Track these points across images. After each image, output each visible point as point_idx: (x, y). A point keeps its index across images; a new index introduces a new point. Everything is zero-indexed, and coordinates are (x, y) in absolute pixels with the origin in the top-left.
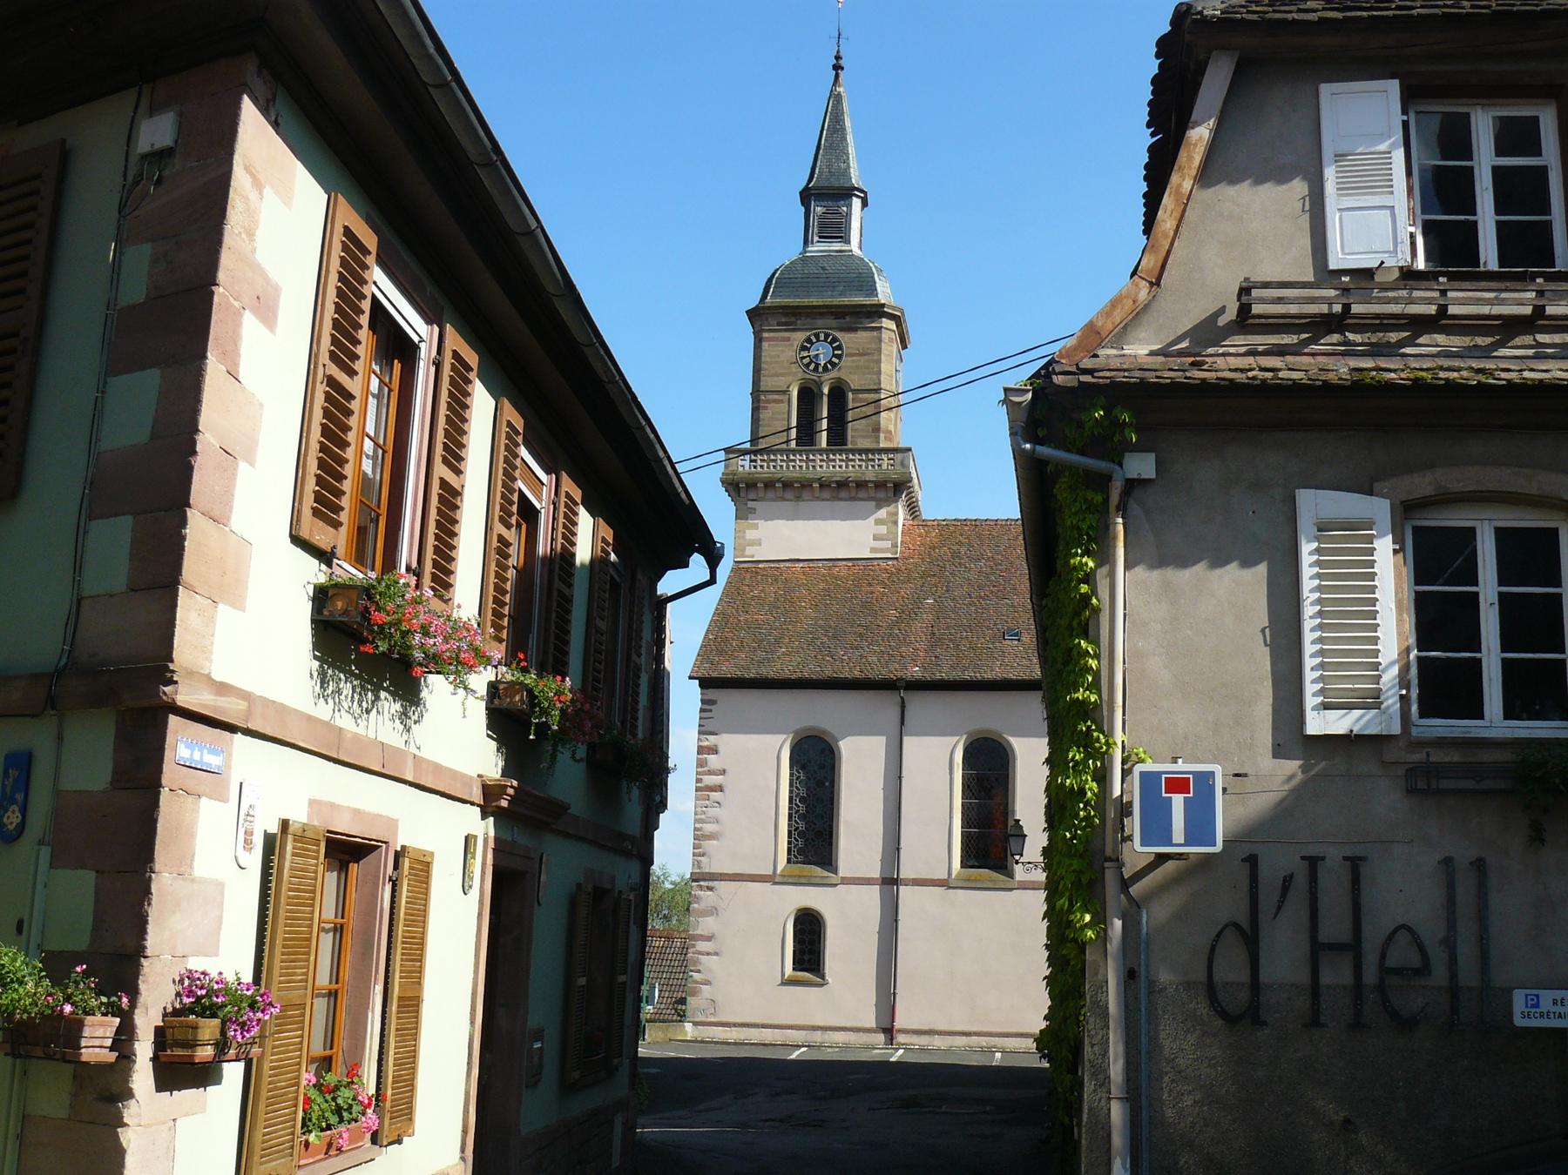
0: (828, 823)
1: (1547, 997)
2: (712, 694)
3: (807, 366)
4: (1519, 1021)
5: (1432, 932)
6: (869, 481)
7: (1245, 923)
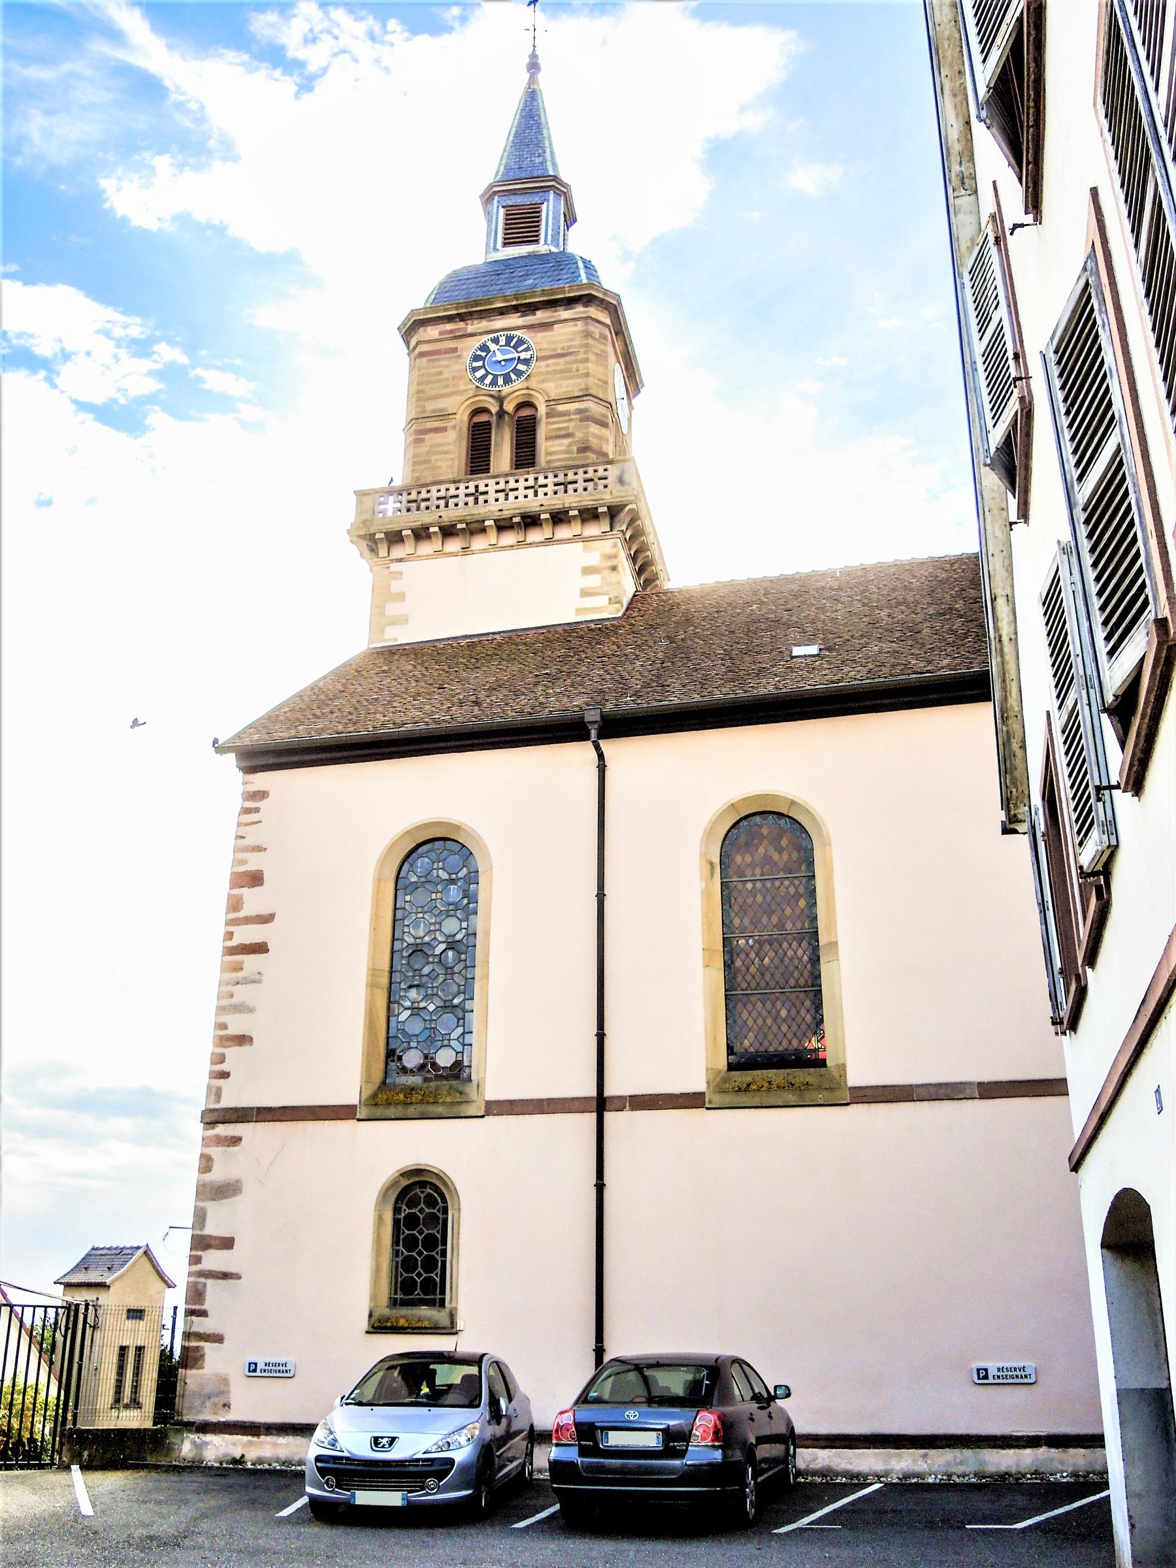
2: (263, 780)
3: (482, 379)
6: (570, 509)
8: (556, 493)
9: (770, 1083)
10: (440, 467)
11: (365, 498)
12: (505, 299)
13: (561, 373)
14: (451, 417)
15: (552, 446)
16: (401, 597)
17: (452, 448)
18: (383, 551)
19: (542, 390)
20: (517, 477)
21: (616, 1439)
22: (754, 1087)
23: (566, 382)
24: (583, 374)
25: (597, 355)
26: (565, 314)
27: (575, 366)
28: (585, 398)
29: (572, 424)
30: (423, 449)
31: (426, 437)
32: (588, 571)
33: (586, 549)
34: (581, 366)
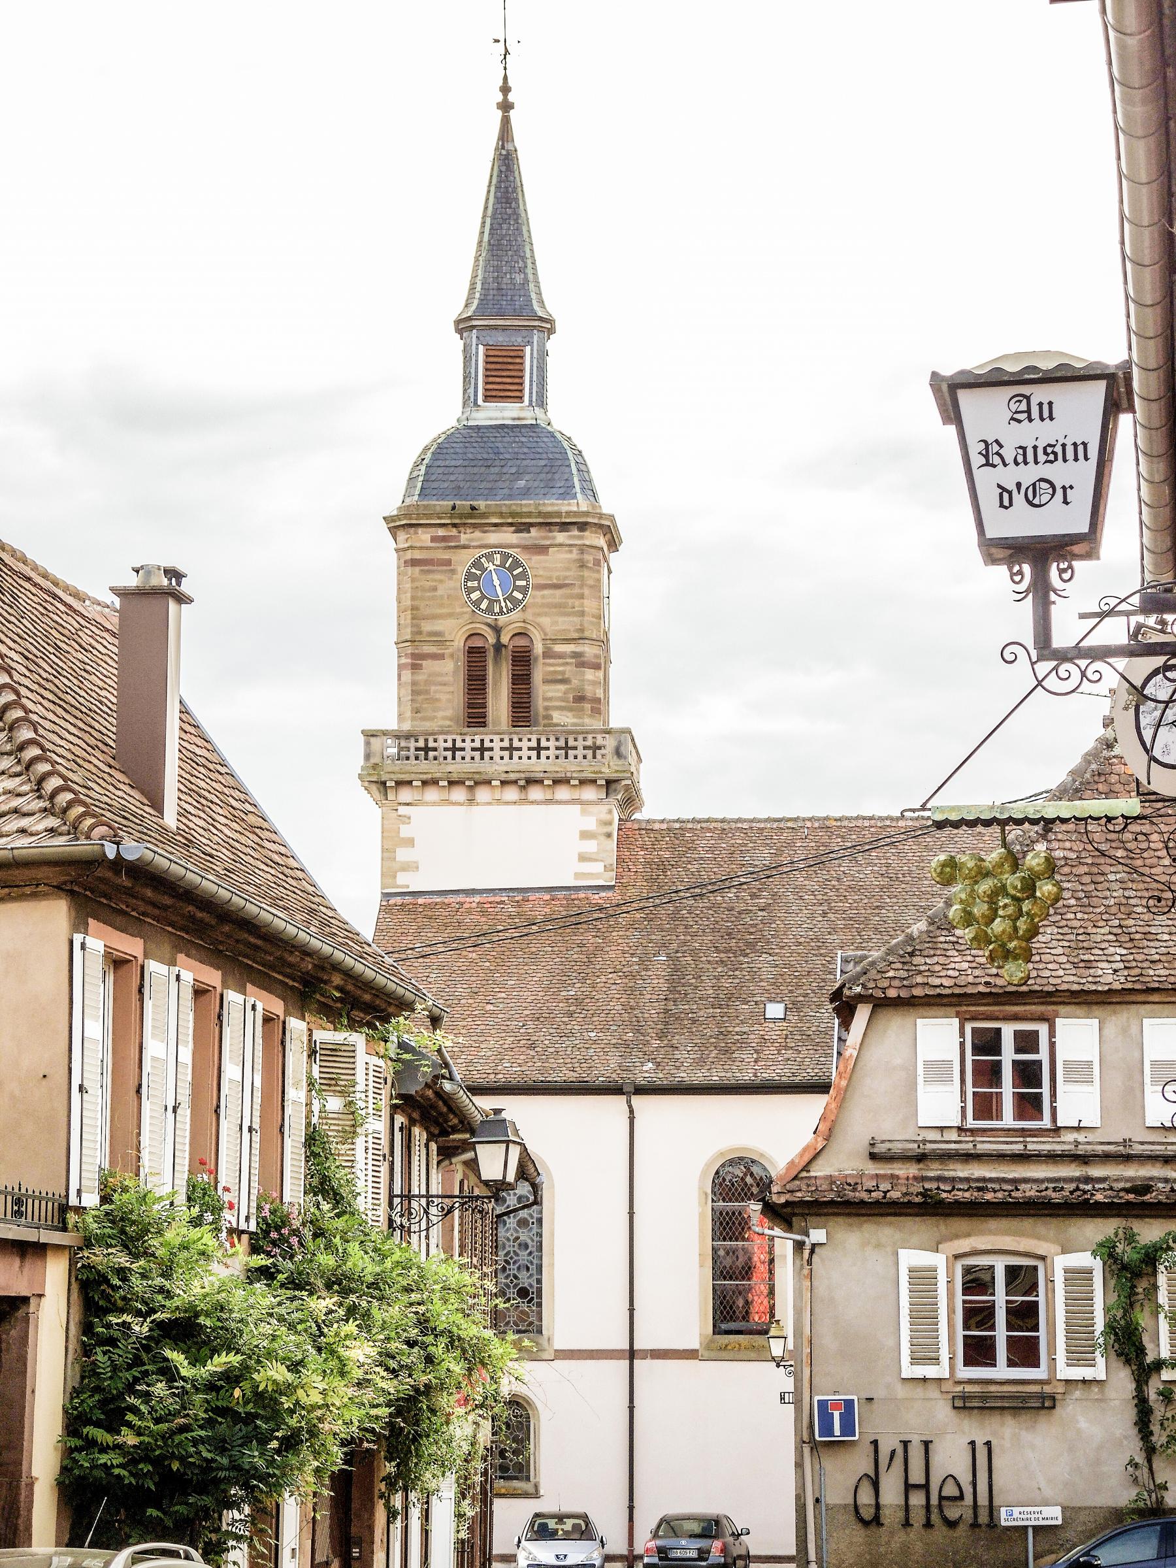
0: (535, 1277)
1: (1016, 1510)
3: (477, 604)
4: (1003, 1523)
5: (965, 1479)
7: (872, 1475)
8: (557, 757)
9: (740, 1345)
10: (438, 700)
11: (372, 740)
12: (501, 515)
13: (556, 607)
14: (448, 643)
15: (549, 691)
16: (410, 842)
17: (450, 679)
18: (391, 796)
19: (538, 624)
20: (520, 736)
21: (678, 1554)
22: (729, 1347)
23: (561, 619)
24: (578, 611)
25: (591, 587)
26: (561, 537)
27: (570, 601)
28: (581, 641)
29: (568, 668)
30: (421, 677)
31: (424, 663)
32: (585, 835)
33: (584, 813)
34: (577, 603)
